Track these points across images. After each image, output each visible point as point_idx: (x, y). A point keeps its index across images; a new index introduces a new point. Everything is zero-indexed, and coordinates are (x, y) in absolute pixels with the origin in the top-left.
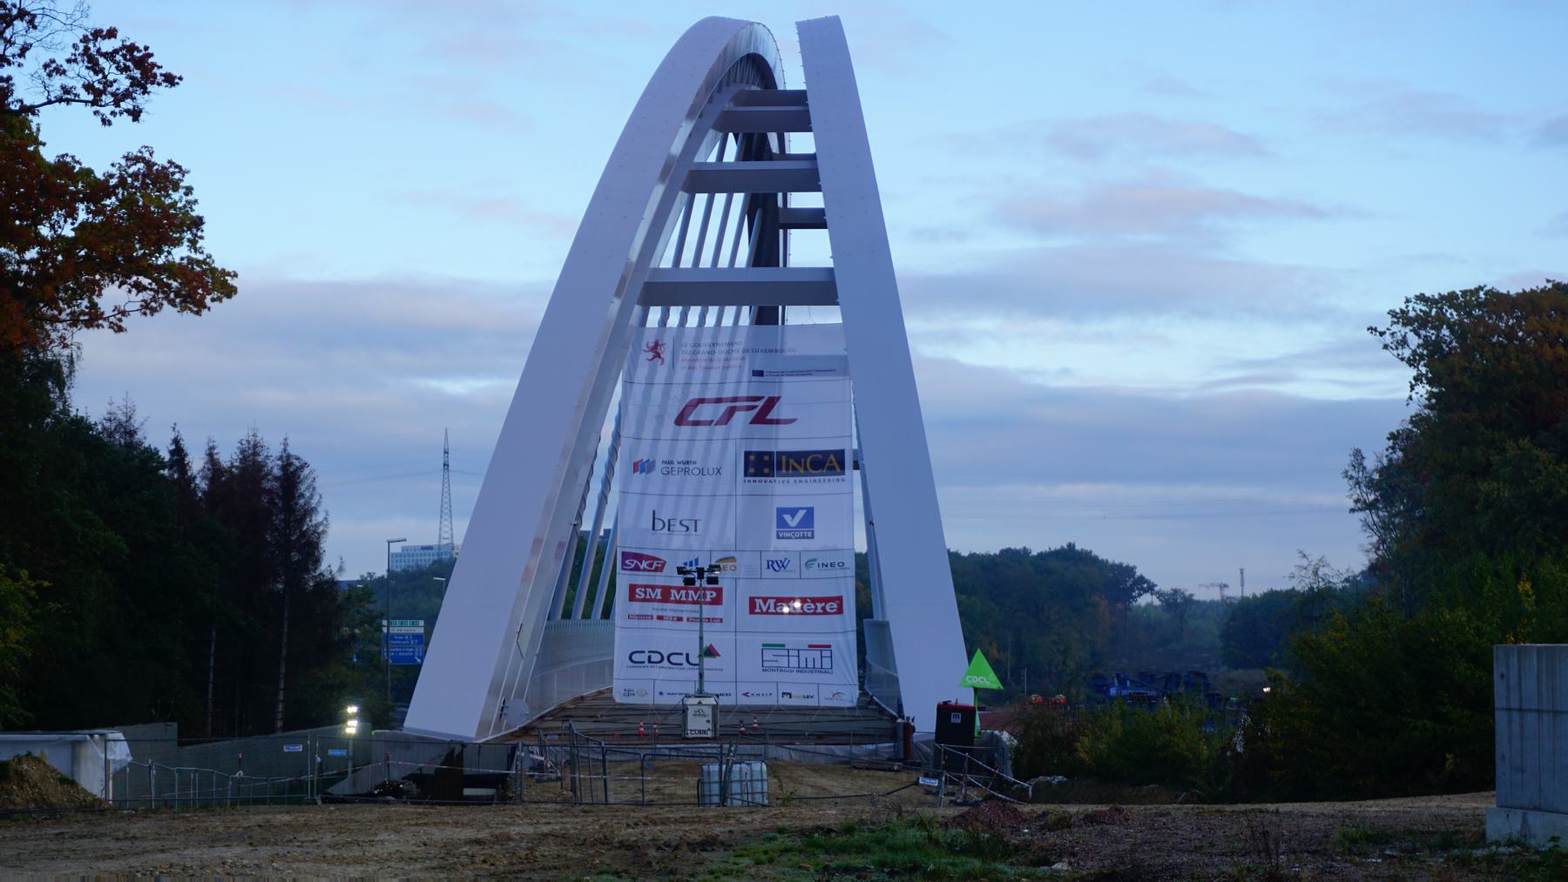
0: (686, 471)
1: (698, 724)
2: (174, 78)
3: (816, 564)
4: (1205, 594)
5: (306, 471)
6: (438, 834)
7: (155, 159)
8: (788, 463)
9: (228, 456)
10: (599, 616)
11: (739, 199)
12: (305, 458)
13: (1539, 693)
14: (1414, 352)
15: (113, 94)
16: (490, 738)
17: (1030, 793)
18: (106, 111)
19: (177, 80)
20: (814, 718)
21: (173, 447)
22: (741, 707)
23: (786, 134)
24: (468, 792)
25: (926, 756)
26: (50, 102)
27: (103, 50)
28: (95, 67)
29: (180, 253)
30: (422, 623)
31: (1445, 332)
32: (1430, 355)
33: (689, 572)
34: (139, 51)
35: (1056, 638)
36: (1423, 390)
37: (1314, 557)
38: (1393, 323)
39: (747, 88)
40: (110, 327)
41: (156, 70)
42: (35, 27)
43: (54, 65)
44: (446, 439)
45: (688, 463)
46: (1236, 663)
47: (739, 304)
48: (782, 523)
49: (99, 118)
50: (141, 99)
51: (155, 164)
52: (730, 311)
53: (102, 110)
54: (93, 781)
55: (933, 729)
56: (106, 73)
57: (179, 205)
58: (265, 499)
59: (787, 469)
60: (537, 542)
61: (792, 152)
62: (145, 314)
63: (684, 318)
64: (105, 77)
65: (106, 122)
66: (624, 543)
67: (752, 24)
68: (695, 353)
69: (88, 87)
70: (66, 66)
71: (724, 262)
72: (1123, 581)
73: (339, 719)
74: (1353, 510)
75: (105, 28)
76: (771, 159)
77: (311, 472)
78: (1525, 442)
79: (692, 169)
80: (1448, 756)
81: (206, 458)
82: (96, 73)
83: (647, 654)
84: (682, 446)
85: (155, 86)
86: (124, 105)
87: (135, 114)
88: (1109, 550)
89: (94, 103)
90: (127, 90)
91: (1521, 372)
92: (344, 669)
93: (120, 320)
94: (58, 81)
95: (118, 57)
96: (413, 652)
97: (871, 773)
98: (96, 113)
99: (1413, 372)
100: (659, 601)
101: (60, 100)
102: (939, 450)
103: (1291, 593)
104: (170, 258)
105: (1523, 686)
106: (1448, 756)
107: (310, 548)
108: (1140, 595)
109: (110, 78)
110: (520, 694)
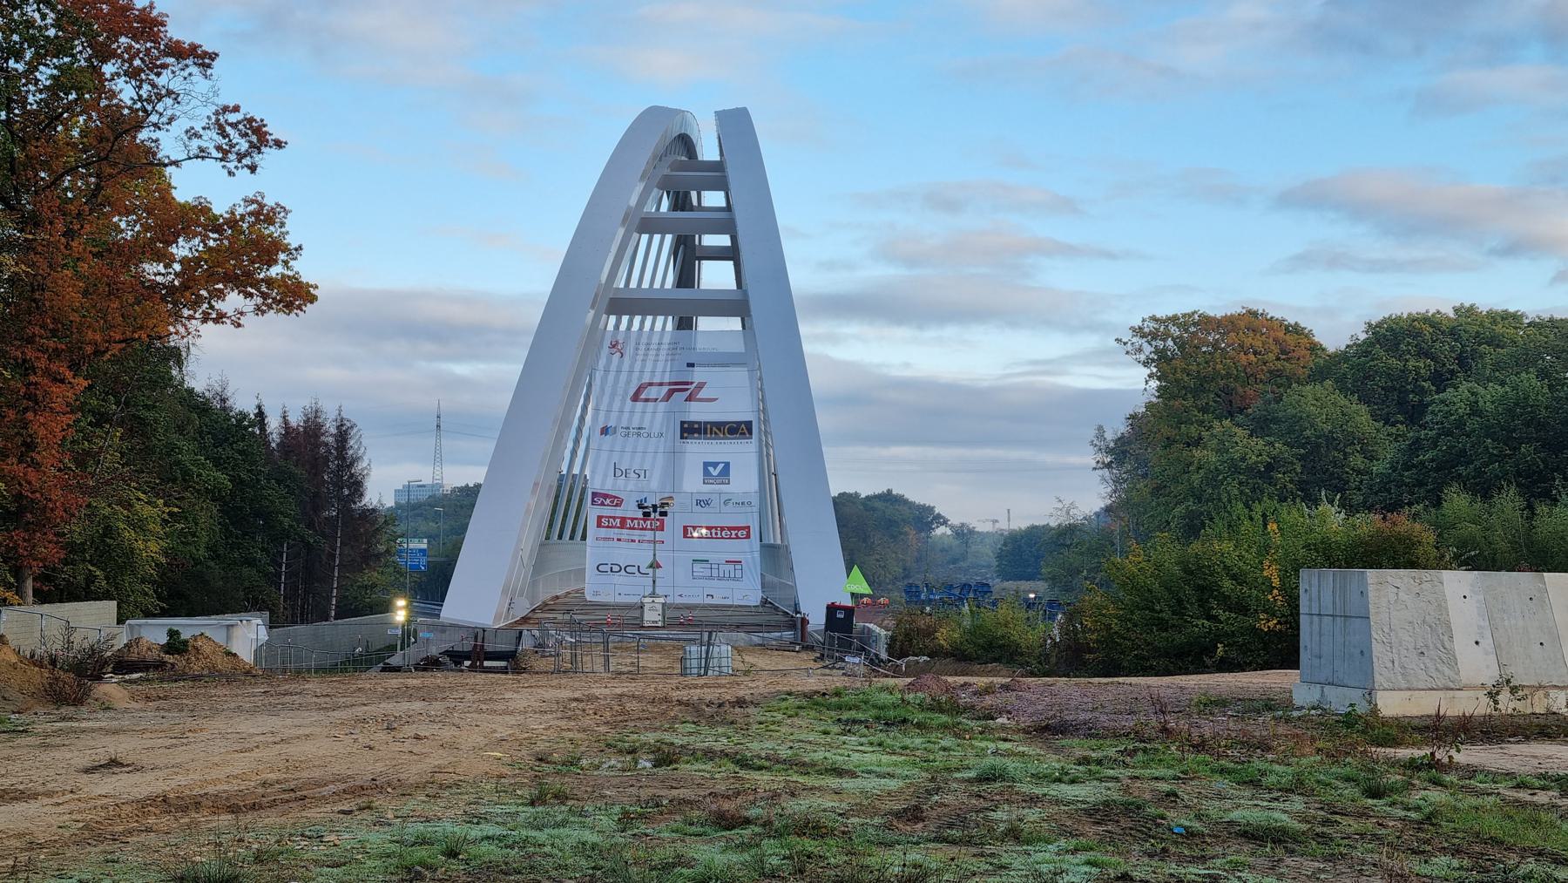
0: (639, 435)
1: (652, 616)
2: (281, 143)
3: (731, 502)
4: (983, 527)
5: (355, 430)
6: (550, 694)
7: (265, 201)
8: (711, 429)
9: (295, 420)
10: (579, 539)
11: (669, 238)
12: (354, 420)
13: (1334, 603)
14: (1148, 358)
15: (237, 154)
16: (501, 625)
17: (904, 669)
18: (231, 165)
19: (283, 144)
20: (729, 613)
21: (257, 411)
22: (677, 604)
23: (702, 192)
24: (486, 663)
25: (817, 641)
26: (190, 158)
27: (230, 121)
28: (224, 135)
29: (276, 271)
30: (425, 541)
31: (1170, 343)
32: (1159, 359)
33: (646, 507)
34: (256, 122)
35: (878, 557)
36: (1154, 384)
37: (1067, 503)
38: (1133, 336)
39: (679, 158)
40: (232, 324)
41: (268, 137)
42: (178, 103)
43: (193, 131)
44: (439, 407)
45: (639, 428)
46: (1006, 577)
47: (666, 314)
48: (706, 473)
49: (226, 171)
50: (257, 158)
51: (265, 205)
52: (660, 319)
53: (227, 164)
54: (246, 653)
55: (824, 621)
56: (231, 138)
57: (275, 235)
58: (322, 450)
59: (711, 433)
60: (536, 484)
61: (706, 205)
62: (257, 314)
63: (642, 323)
64: (230, 141)
65: (230, 173)
66: (595, 485)
67: (684, 111)
68: (658, 349)
69: (219, 148)
70: (201, 132)
71: (657, 285)
72: (925, 518)
73: (386, 607)
74: (1095, 469)
75: (231, 105)
76: (692, 210)
77: (359, 430)
78: (1227, 423)
79: (643, 216)
80: (1219, 645)
81: (281, 420)
82: (224, 137)
83: (610, 566)
84: (637, 417)
85: (268, 148)
86: (244, 161)
87: (253, 168)
88: (916, 496)
89: (221, 160)
90: (247, 151)
91: (1224, 372)
92: (376, 574)
93: (239, 319)
94: (195, 143)
95: (241, 127)
96: (419, 562)
97: (780, 653)
98: (223, 167)
99: (1148, 372)
100: (619, 528)
101: (197, 157)
102: (825, 421)
103: (1046, 528)
104: (268, 273)
105: (1322, 595)
106: (1219, 645)
107: (357, 487)
108: (938, 527)
109: (234, 141)
110: (521, 595)
